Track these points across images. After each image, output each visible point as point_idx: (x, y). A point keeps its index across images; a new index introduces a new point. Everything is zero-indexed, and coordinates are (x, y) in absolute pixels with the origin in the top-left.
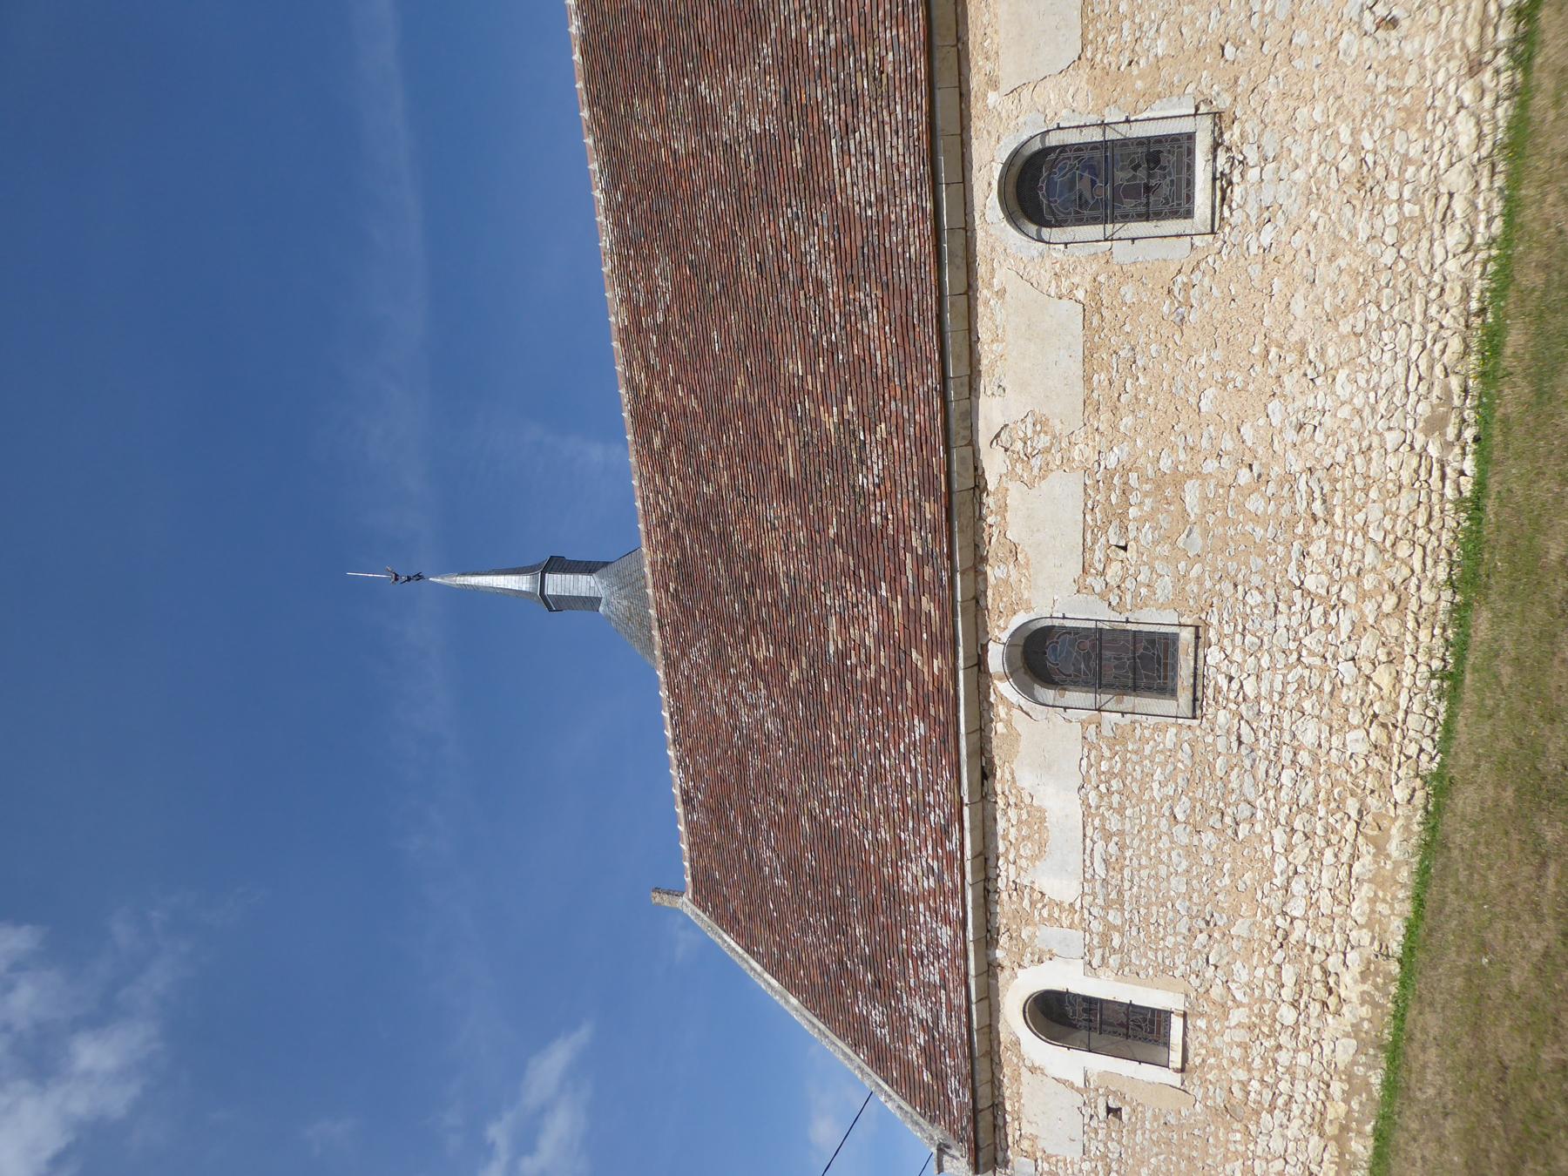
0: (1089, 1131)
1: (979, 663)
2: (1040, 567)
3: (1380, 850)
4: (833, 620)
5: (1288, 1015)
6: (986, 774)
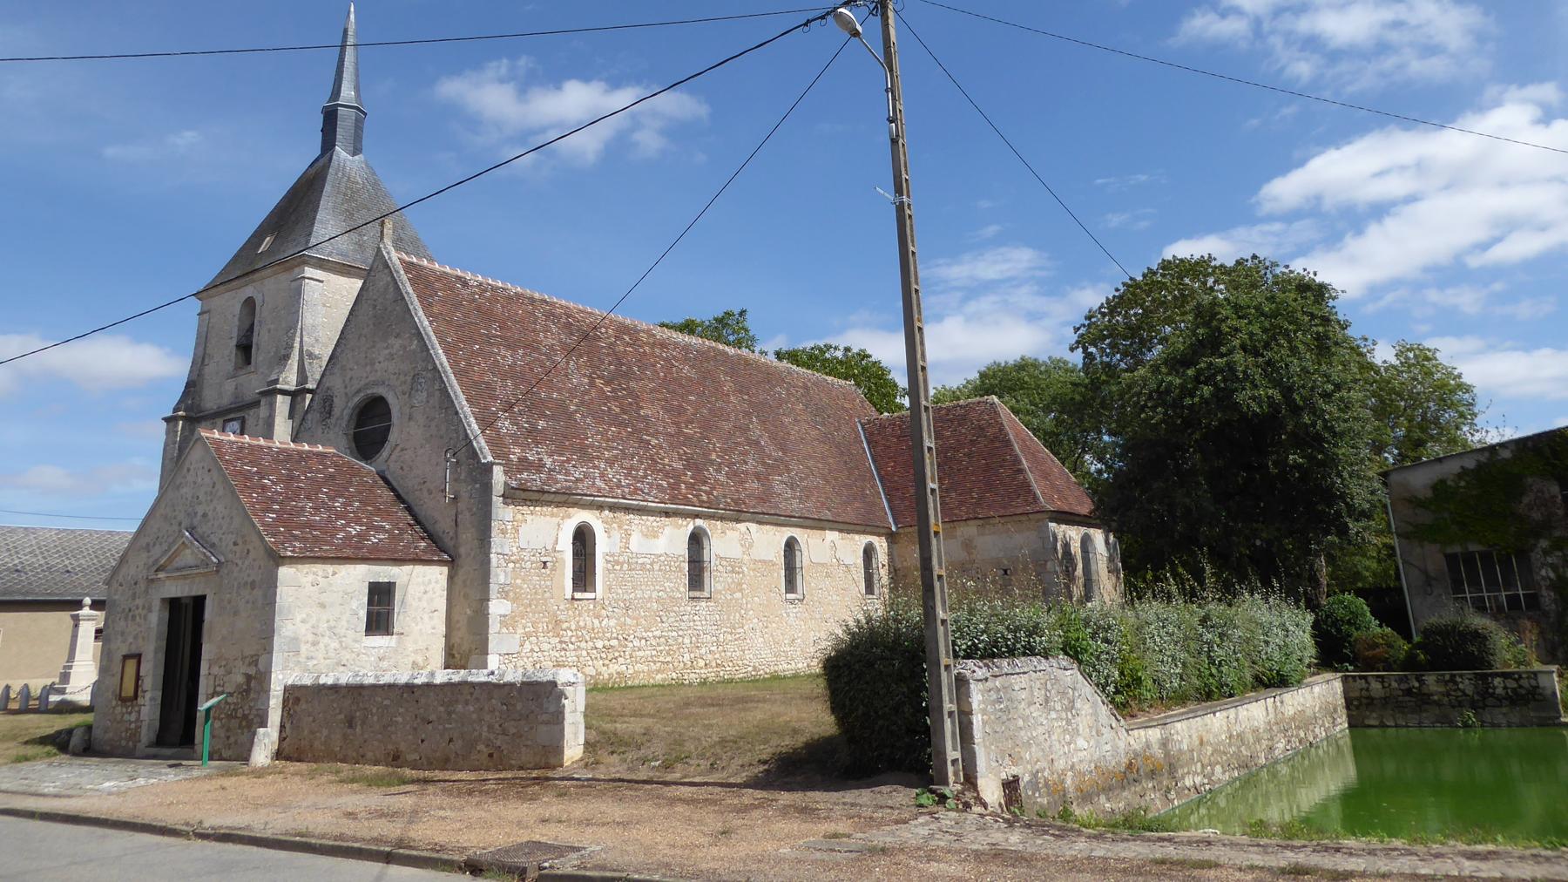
0: (535, 552)
1: (697, 516)
2: (725, 541)
3: (658, 671)
4: (282, 403)
5: (600, 644)
6: (667, 514)
